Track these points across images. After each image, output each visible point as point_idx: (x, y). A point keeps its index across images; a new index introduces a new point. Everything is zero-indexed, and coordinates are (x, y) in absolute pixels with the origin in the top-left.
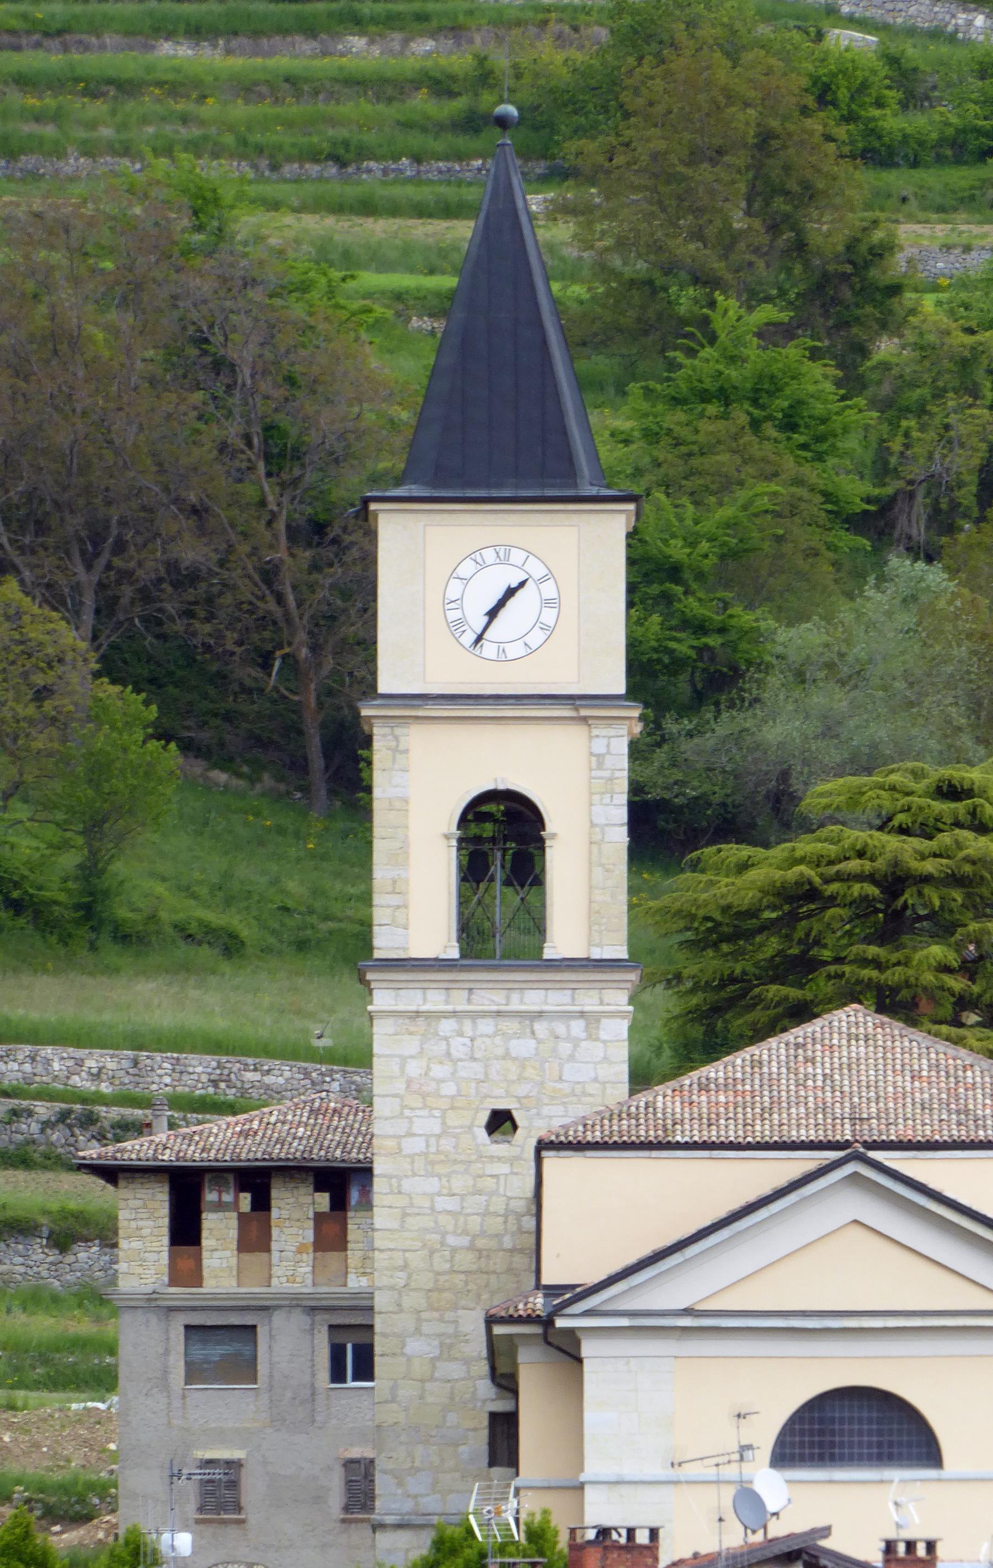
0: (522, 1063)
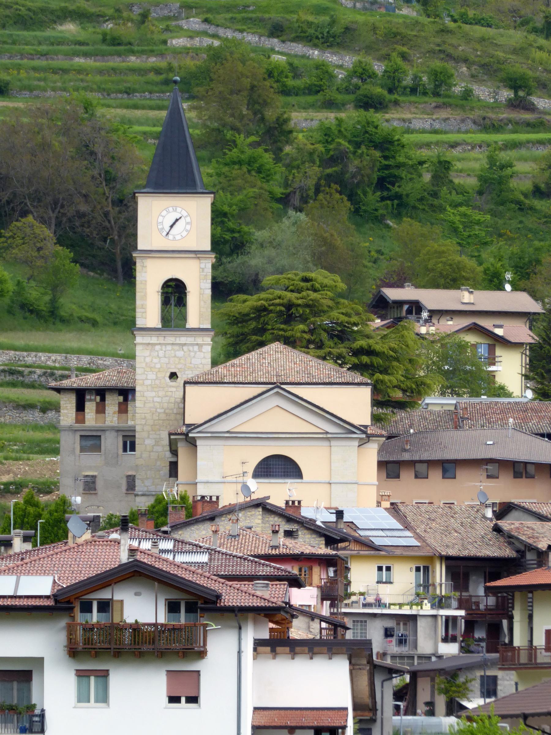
0: (180, 358)
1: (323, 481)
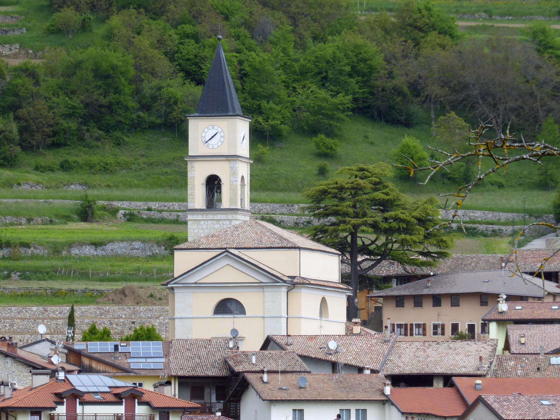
1: (259, 315)
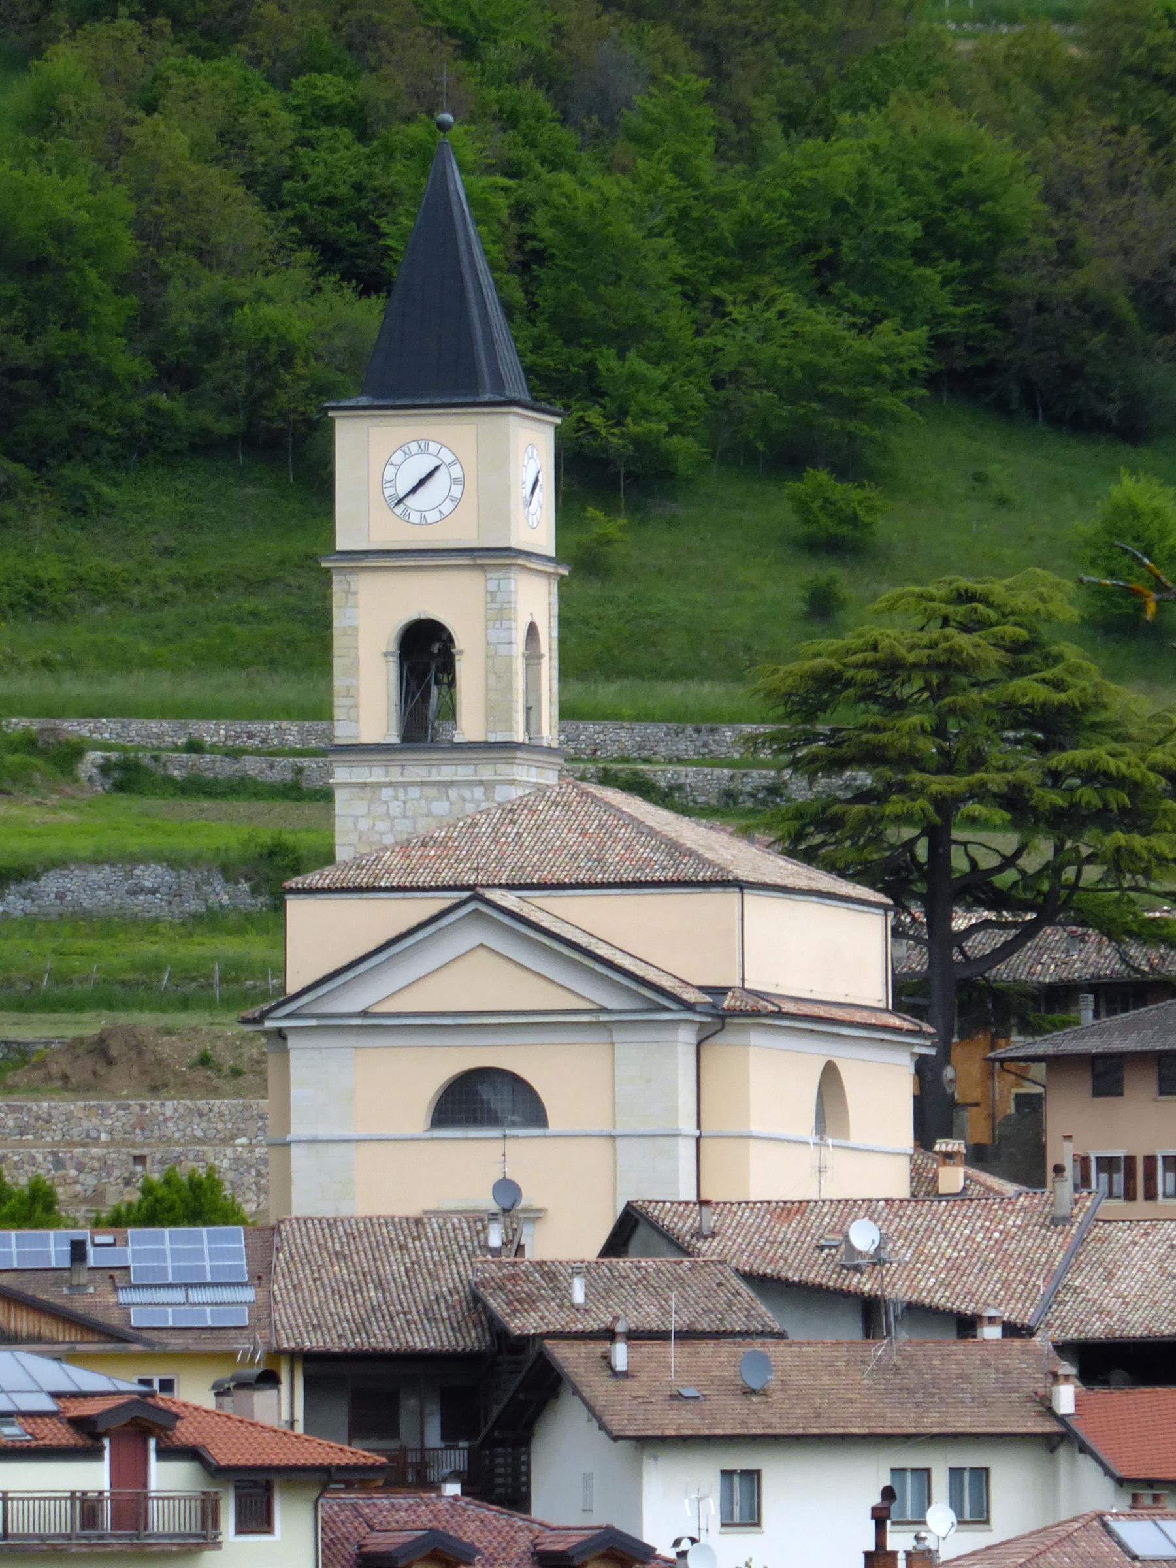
1: (595, 1129)
